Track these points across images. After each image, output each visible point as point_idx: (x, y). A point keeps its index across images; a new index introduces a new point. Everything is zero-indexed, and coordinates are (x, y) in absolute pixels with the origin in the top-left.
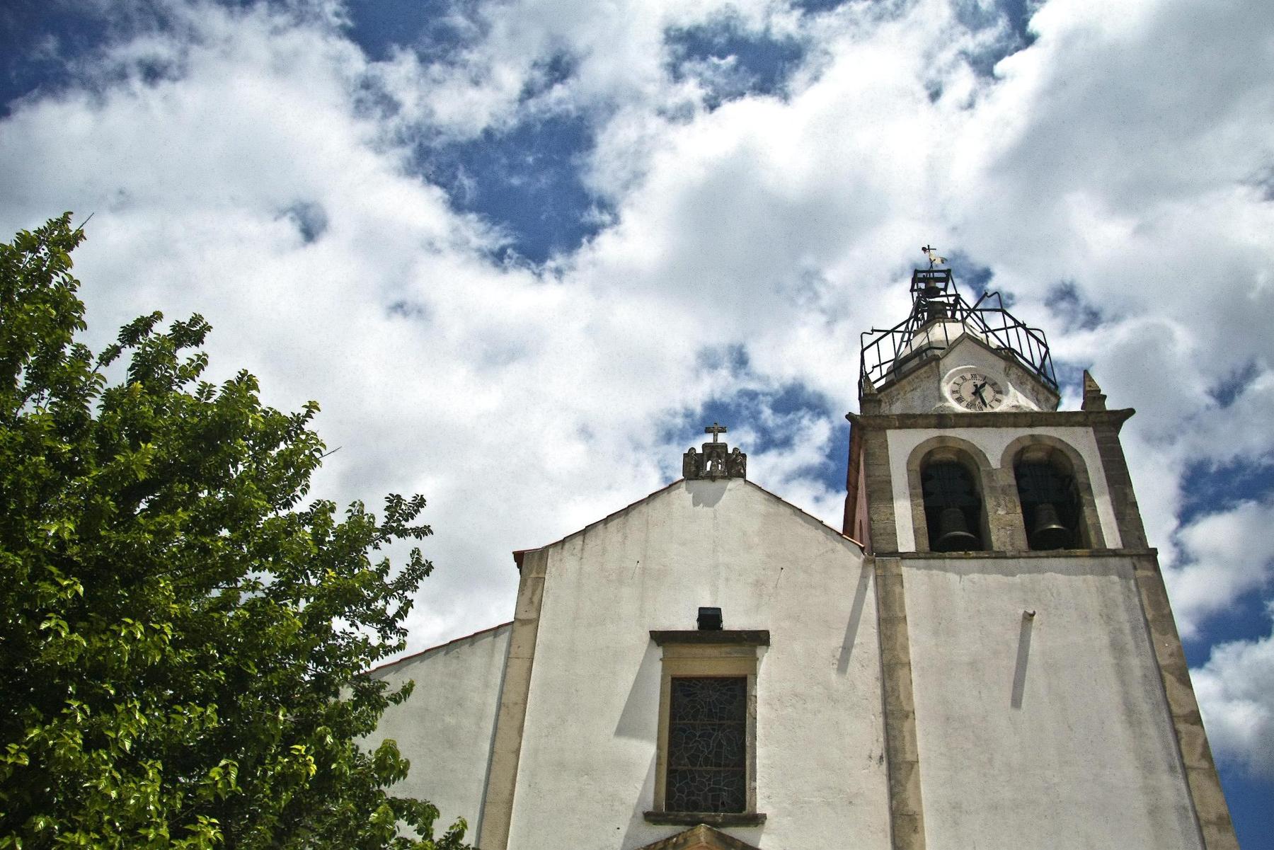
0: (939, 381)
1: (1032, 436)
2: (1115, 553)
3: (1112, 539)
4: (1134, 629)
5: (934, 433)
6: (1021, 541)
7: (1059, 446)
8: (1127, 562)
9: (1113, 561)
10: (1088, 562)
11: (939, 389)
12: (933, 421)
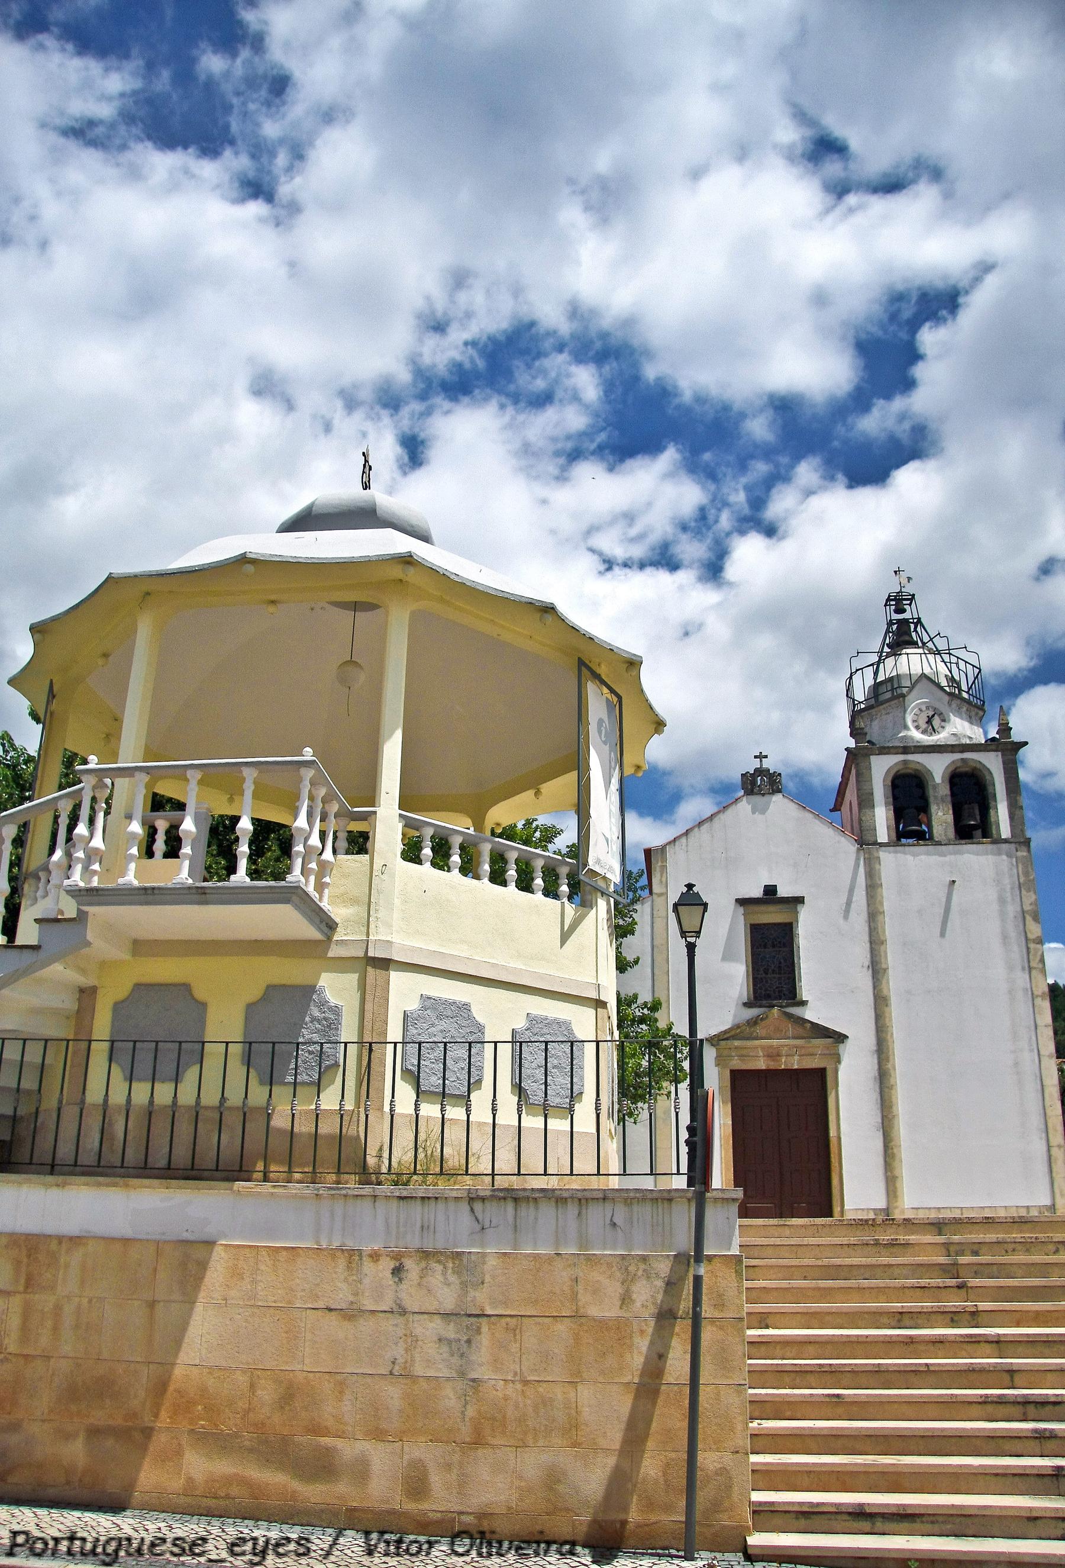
0: (905, 711)
1: (962, 759)
2: (1006, 841)
3: (1005, 832)
4: (1012, 888)
5: (901, 757)
6: (951, 832)
7: (978, 766)
8: (1013, 846)
9: (1004, 846)
10: (990, 847)
11: (904, 719)
12: (900, 750)
